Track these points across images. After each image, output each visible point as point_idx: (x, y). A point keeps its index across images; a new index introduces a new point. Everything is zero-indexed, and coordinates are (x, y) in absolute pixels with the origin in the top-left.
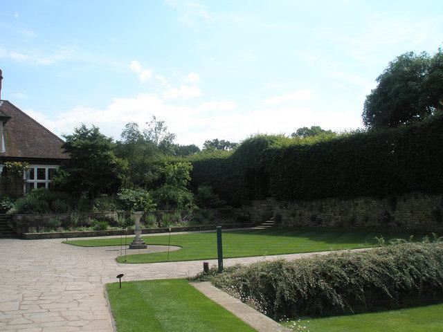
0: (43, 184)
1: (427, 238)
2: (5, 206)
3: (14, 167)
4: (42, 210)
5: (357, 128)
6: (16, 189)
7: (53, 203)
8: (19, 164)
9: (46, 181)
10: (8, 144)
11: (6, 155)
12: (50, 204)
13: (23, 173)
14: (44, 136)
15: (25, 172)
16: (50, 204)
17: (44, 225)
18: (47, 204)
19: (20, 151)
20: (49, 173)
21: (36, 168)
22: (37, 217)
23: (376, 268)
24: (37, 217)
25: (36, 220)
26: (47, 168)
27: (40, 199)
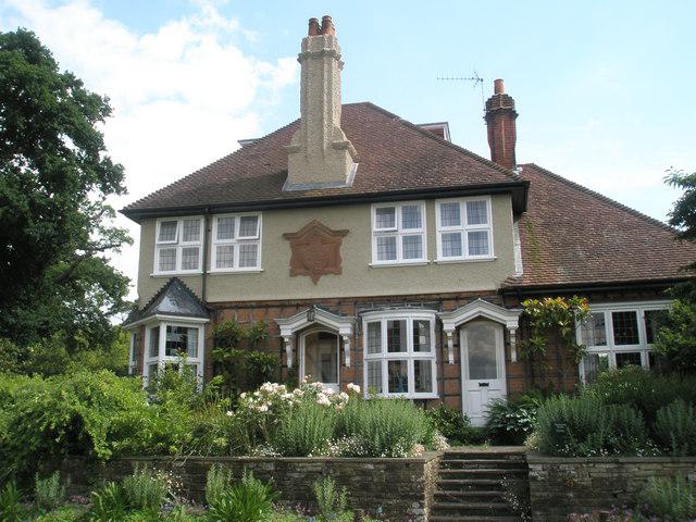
0: (635, 358)
1: (115, 272)
2: (526, 424)
3: (547, 314)
4: (619, 443)
5: (101, 93)
6: (560, 376)
7: (660, 413)
8: (561, 302)
9: (642, 347)
10: (529, 256)
11: (527, 282)
12: (650, 417)
13: (572, 326)
14: (624, 228)
15: (578, 323)
16: (650, 417)
17: (631, 506)
18: (638, 421)
19: (560, 269)
20: (648, 323)
21: (608, 311)
22: (603, 468)
23: (316, 435)
24: (603, 468)
25: (598, 481)
26: (640, 309)
27: (615, 400)
